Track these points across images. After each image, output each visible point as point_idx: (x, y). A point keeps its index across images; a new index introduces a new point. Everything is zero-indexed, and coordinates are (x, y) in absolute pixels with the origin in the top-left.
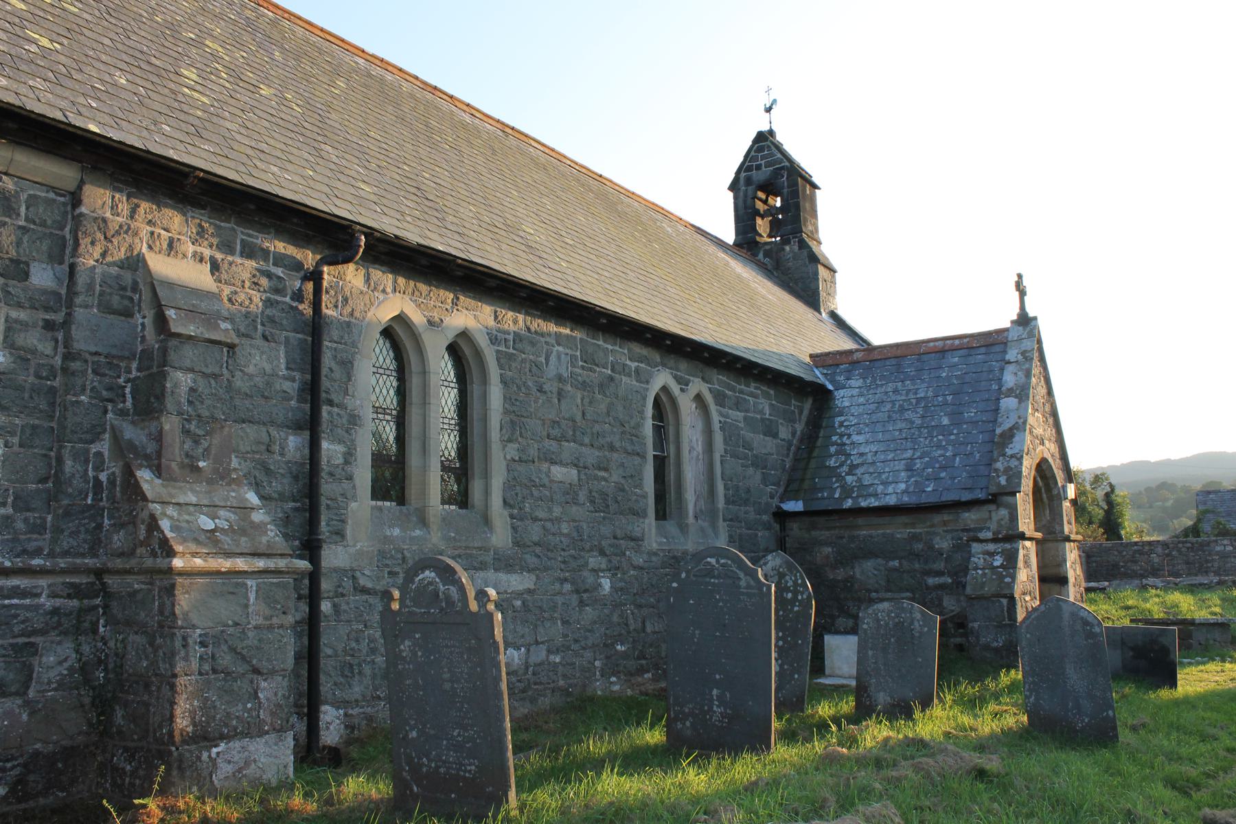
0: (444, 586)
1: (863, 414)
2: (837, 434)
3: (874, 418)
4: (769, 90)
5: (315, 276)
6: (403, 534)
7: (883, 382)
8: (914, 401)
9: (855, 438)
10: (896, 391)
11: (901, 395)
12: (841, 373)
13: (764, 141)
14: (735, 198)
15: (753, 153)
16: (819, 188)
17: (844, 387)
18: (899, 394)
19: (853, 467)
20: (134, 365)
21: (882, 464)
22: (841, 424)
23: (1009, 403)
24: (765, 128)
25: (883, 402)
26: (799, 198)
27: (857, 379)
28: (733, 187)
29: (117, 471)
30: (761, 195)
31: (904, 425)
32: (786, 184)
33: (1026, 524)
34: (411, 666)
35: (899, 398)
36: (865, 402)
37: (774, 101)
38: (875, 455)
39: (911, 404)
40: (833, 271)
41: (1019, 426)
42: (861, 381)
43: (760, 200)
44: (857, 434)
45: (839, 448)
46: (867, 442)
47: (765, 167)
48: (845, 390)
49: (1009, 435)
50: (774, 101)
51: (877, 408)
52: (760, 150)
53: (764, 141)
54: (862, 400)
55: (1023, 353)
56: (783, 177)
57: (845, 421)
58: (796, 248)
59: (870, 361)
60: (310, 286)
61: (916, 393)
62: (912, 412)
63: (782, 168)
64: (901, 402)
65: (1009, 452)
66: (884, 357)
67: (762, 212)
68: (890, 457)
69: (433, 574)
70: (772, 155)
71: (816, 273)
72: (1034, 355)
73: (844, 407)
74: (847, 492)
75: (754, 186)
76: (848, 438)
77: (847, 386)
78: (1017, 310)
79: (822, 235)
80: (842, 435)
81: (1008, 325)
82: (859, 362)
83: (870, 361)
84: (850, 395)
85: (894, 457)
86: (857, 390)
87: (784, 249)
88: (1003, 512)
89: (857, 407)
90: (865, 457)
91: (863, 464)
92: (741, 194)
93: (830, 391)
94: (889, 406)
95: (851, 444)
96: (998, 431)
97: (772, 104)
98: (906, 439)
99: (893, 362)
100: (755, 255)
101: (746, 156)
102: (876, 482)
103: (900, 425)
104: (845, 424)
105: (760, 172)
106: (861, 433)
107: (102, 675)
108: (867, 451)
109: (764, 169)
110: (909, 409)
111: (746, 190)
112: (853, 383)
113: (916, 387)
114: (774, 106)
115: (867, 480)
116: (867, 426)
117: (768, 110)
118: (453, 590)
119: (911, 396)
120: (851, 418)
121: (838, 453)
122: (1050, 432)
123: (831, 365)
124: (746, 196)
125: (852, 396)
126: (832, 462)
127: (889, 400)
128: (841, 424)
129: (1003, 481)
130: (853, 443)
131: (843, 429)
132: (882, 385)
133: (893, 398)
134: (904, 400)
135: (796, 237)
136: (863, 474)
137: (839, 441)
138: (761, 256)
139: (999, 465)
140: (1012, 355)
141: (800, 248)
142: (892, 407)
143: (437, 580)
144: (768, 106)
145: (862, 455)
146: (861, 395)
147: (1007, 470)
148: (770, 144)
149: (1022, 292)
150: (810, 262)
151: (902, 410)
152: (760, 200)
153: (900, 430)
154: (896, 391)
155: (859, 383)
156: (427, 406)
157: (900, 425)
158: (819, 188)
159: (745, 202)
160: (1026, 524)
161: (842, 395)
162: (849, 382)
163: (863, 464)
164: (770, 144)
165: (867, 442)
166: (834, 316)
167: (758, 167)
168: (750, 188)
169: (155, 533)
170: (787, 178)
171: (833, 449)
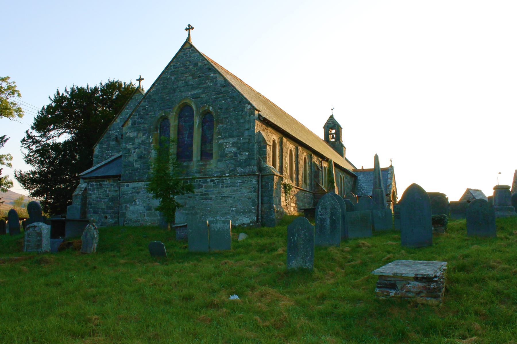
5: (322, 162)
6: (37, 174)
13: (332, 117)
14: (324, 130)
19: (363, 190)
23: (389, 180)
28: (324, 127)
30: (330, 130)
33: (391, 199)
37: (334, 108)
40: (345, 148)
41: (391, 184)
46: (365, 186)
49: (389, 185)
50: (334, 108)
52: (331, 120)
53: (332, 117)
55: (391, 172)
58: (338, 143)
65: (389, 188)
70: (334, 121)
71: (343, 149)
72: (392, 173)
74: (362, 193)
78: (390, 164)
79: (343, 140)
81: (389, 167)
88: (388, 197)
92: (326, 129)
96: (388, 185)
100: (329, 143)
115: (366, 192)
117: (332, 110)
122: (394, 186)
124: (327, 130)
126: (359, 189)
129: (388, 192)
138: (330, 144)
139: (388, 190)
140: (389, 172)
147: (389, 191)
149: (391, 161)
159: (327, 131)
160: (391, 199)
166: (346, 158)
167: (330, 124)
171: (359, 186)
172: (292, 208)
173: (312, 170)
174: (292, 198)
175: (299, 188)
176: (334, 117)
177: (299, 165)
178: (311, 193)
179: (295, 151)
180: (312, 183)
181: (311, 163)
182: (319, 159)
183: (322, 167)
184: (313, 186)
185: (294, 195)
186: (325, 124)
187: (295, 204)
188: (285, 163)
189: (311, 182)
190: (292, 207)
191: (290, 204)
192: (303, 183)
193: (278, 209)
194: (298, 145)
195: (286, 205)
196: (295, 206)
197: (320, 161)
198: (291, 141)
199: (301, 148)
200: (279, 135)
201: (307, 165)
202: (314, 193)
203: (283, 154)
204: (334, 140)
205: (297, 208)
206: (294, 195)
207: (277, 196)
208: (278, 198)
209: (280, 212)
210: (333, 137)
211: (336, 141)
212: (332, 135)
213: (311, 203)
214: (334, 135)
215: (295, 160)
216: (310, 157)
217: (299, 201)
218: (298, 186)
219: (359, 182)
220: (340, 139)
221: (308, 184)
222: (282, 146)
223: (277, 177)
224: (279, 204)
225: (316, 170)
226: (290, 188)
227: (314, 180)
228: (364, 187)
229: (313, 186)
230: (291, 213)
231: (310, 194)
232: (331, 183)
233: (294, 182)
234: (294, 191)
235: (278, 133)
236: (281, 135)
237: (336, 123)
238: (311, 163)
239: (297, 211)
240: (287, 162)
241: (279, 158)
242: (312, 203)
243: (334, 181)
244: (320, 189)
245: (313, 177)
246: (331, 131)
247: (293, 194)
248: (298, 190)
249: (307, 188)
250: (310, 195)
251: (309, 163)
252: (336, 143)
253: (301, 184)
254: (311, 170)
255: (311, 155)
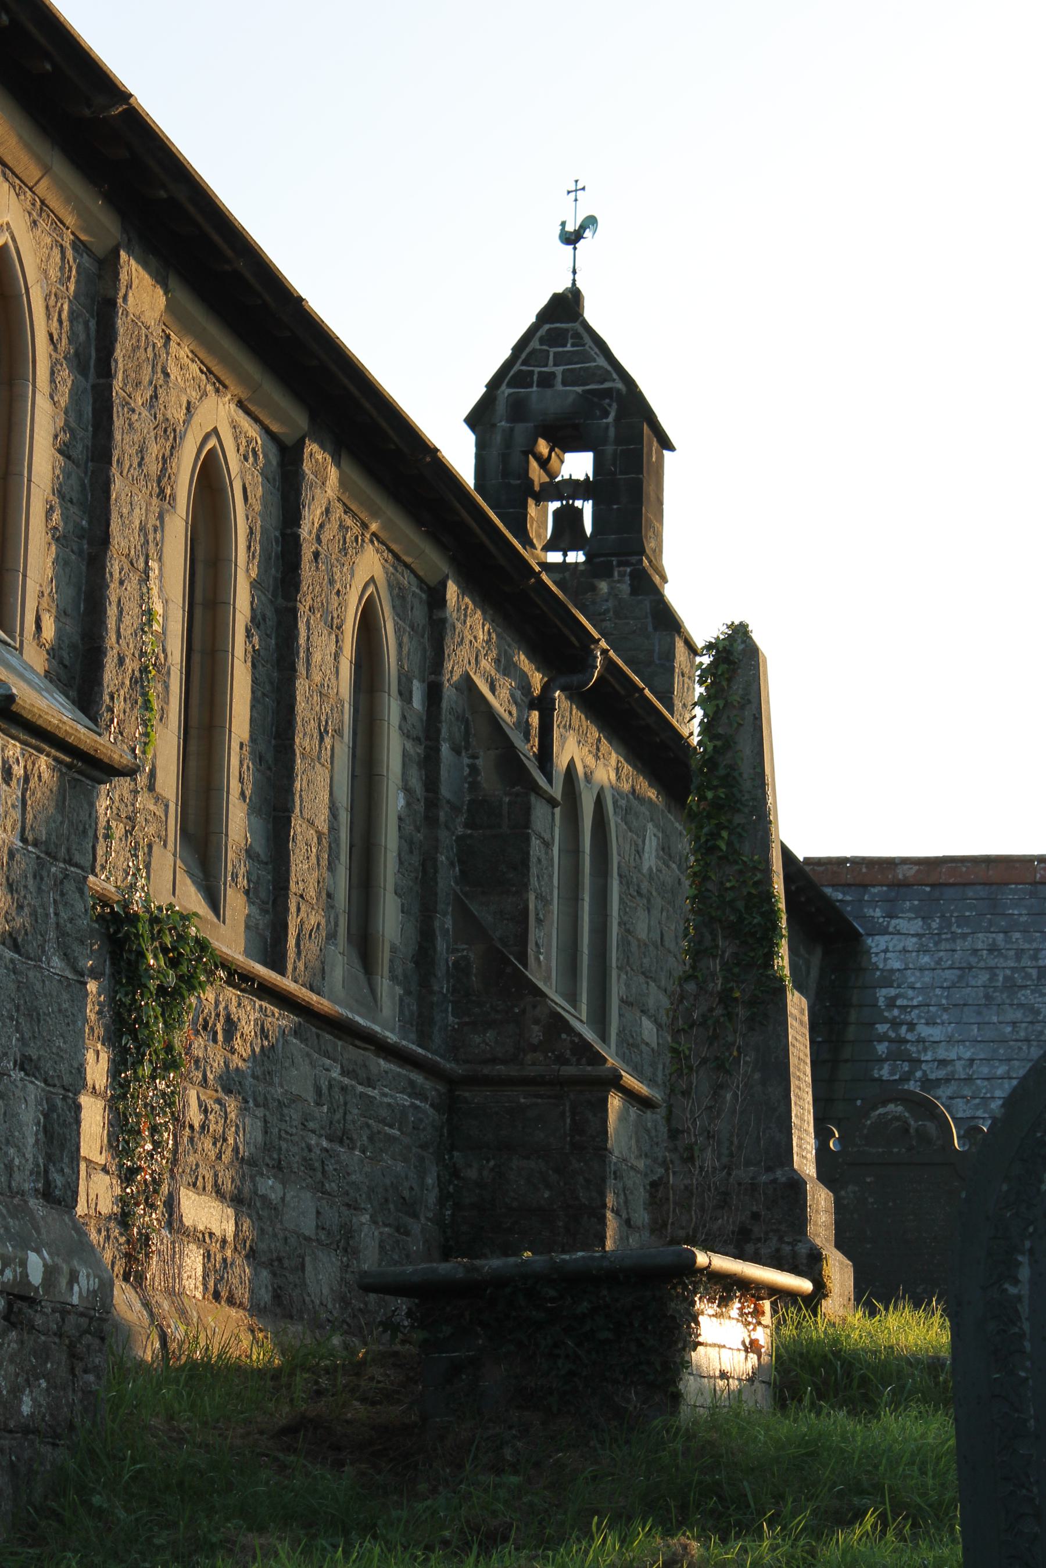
0: (916, 1121)
1: (933, 988)
2: (885, 1021)
3: (957, 996)
4: (576, 190)
7: (966, 930)
8: (1034, 973)
9: (924, 1031)
10: (993, 949)
11: (1006, 958)
12: (873, 903)
15: (535, 344)
16: (671, 447)
17: (884, 932)
18: (1001, 955)
20: (461, 819)
21: (986, 1083)
22: (891, 1003)
24: (561, 285)
25: (971, 968)
26: (642, 473)
27: (910, 919)
29: (472, 955)
30: (543, 447)
31: (1019, 1015)
32: (612, 432)
34: (855, 1216)
35: (1001, 962)
36: (933, 965)
37: (590, 222)
38: (971, 1065)
39: (1028, 976)
42: (919, 922)
43: (538, 458)
44: (927, 1024)
45: (894, 1046)
46: (950, 1041)
47: (564, 384)
48: (887, 937)
50: (590, 222)
51: (961, 978)
52: (555, 338)
54: (925, 959)
56: (606, 414)
57: (897, 997)
58: (625, 588)
59: (932, 885)
60: (535, 717)
61: (1035, 958)
62: (1033, 992)
63: (608, 393)
64: (1008, 972)
66: (959, 880)
67: (537, 488)
68: (1000, 1071)
69: (900, 1108)
70: (586, 357)
73: (892, 971)
75: (530, 425)
76: (908, 1030)
77: (891, 929)
80: (895, 1024)
82: (909, 885)
83: (932, 885)
84: (900, 947)
85: (1008, 1072)
86: (914, 940)
87: (594, 588)
89: (918, 973)
90: (949, 1068)
91: (948, 1080)
92: (498, 438)
93: (861, 935)
94: (984, 977)
95: (918, 1041)
97: (583, 227)
98: (1027, 1040)
99: (982, 891)
101: (519, 348)
102: (980, 1113)
103: (1013, 1015)
104: (899, 1002)
105: (549, 392)
106: (935, 1023)
107: (449, 1212)
108: (953, 1056)
109: (559, 387)
110: (1026, 987)
111: (512, 430)
112: (901, 924)
113: (1035, 945)
114: (588, 233)
116: (945, 1010)
117: (571, 239)
118: (931, 1127)
119: (1026, 962)
120: (910, 993)
121: (893, 1056)
123: (849, 885)
125: (905, 950)
126: (885, 1072)
127: (982, 964)
128: (891, 1003)
130: (920, 1040)
131: (896, 1012)
132: (964, 936)
133: (992, 963)
134: (1012, 969)
135: (627, 564)
136: (951, 1098)
137: (892, 1035)
141: (635, 591)
142: (991, 980)
143: (907, 1114)
144: (570, 228)
145: (943, 1063)
146: (922, 950)
148: (581, 330)
150: (655, 629)
151: (1011, 987)
152: (538, 458)
153: (1014, 1024)
154: (993, 949)
155: (917, 926)
156: (580, 902)
157: (1013, 1015)
158: (671, 447)
159: (505, 457)
161: (883, 947)
162: (894, 922)
163: (948, 1080)
164: (581, 330)
165: (950, 1041)
167: (546, 381)
168: (520, 428)
169: (564, 1036)
170: (617, 419)
172: (193, 1261)
173: (445, 791)
174: (194, 1116)
175: (287, 983)
176: (594, 314)
177: (301, 686)
178: (418, 1078)
179: (257, 492)
180: (441, 945)
181: (434, 693)
182: (523, 661)
183: (545, 756)
184: (442, 986)
185: (230, 1083)
186: (494, 385)
187: (238, 1201)
188: (132, 610)
189: (426, 935)
190: (203, 1238)
191: (171, 1204)
192: (332, 936)
193: (35, 1266)
194: (301, 421)
195: (124, 1219)
196: (230, 1228)
197: (525, 686)
198: (228, 344)
199: (333, 474)
200: (81, 212)
201: (392, 709)
202: (452, 1082)
203: (119, 487)
204: (576, 557)
205: (252, 1255)
206: (230, 1083)
207: (25, 1064)
208: (34, 1089)
209: (64, 1310)
210: (569, 519)
211: (596, 566)
212: (554, 506)
213: (409, 1207)
214: (587, 508)
215: (256, 620)
216: (419, 614)
217: (277, 1167)
218: (276, 961)
219: (883, 994)
220: (642, 552)
221: (384, 957)
222: (105, 369)
223: (43, 762)
224: (47, 1195)
225: (489, 781)
226: (189, 982)
227: (463, 914)
228: (942, 1053)
229: (442, 986)
230: (177, 1331)
231: (414, 1091)
232: (727, 948)
233: (236, 903)
234: (231, 1027)
235: (61, 168)
236: (110, 225)
237: (606, 377)
238: (434, 693)
239: (256, 1309)
240: (158, 607)
241: (59, 539)
242: (432, 1198)
243: (772, 915)
244: (536, 1034)
245: (447, 880)
246: (544, 463)
247: (216, 1058)
248: (280, 1020)
249: (371, 1002)
250: (405, 1100)
251: (405, 696)
252: (603, 586)
253: (311, 948)
254: (431, 784)
255: (436, 598)
